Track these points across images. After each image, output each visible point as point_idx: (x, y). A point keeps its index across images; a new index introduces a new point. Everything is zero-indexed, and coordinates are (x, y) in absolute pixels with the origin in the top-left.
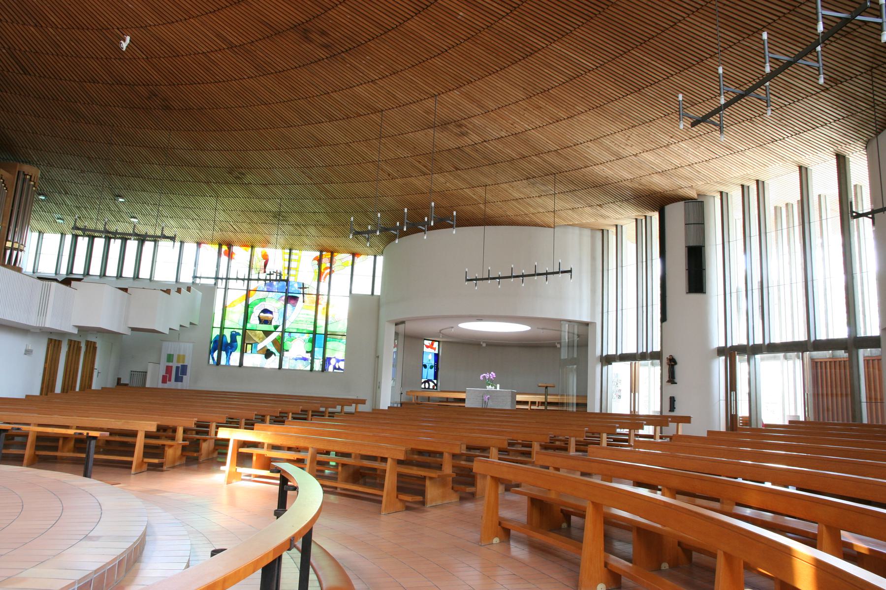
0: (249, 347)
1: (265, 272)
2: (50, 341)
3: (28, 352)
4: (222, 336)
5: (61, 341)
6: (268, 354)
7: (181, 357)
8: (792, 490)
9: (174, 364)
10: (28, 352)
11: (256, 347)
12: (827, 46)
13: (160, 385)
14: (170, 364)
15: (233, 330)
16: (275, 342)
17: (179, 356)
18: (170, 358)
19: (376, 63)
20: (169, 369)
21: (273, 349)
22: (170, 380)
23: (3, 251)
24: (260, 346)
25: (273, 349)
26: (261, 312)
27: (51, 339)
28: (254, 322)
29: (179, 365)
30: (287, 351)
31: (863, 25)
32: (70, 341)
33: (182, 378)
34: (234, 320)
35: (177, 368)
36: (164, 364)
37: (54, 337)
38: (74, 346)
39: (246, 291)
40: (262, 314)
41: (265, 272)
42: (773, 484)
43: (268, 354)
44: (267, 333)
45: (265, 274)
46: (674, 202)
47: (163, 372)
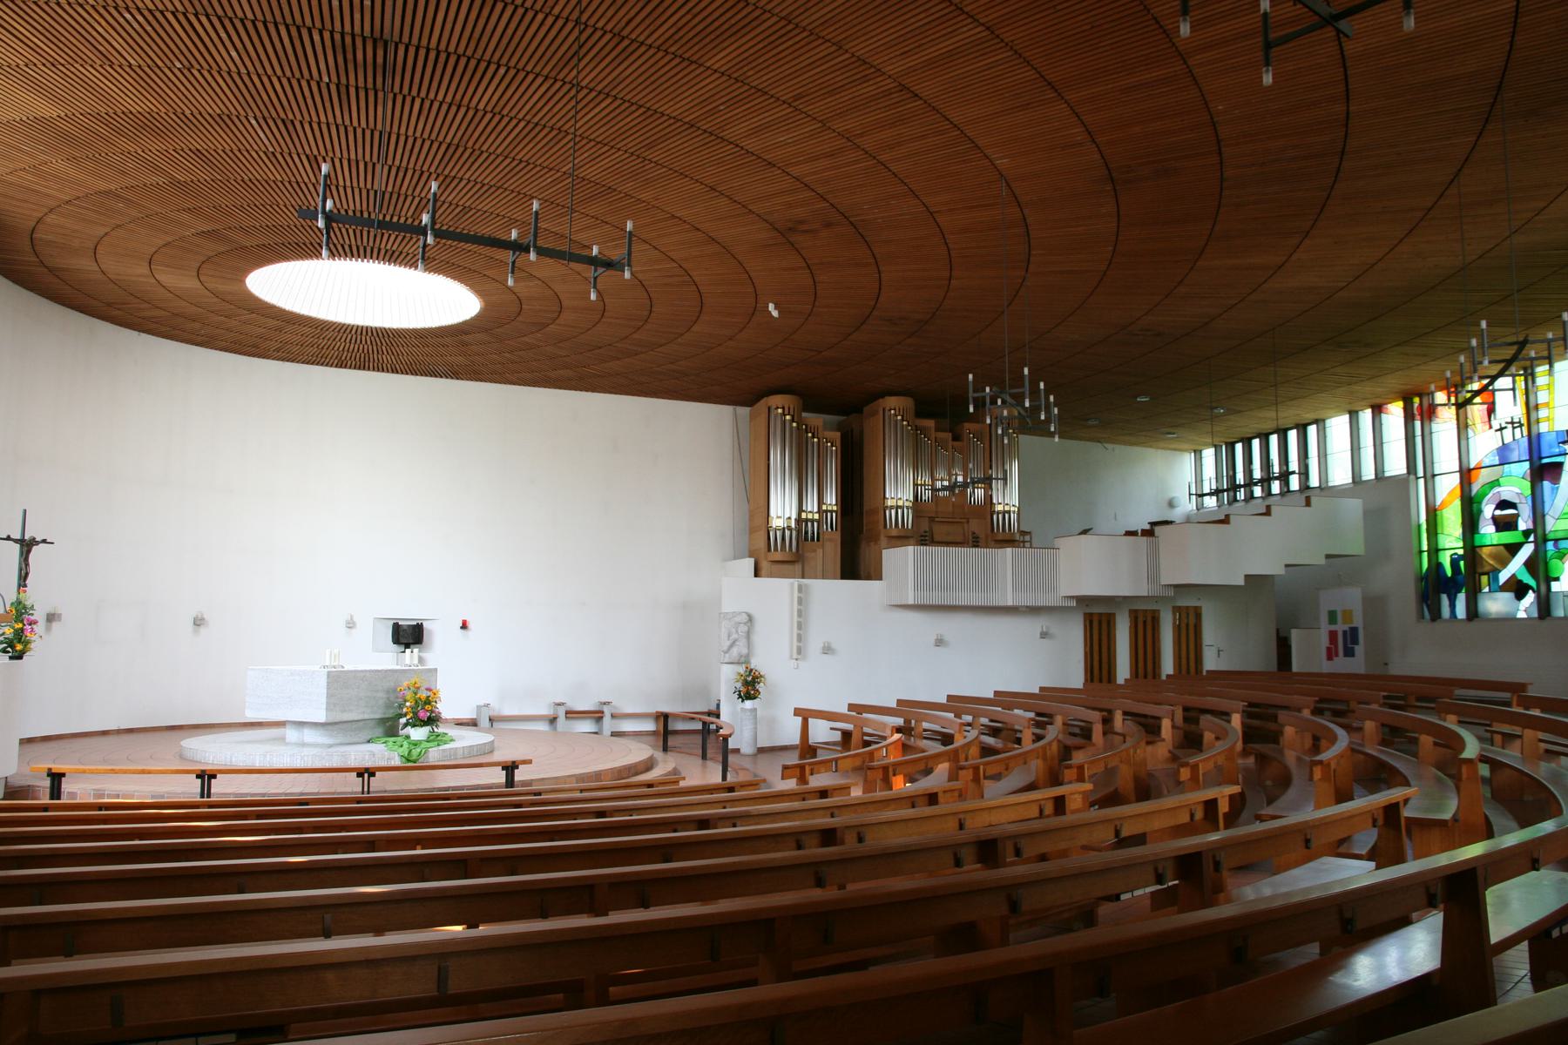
0: (1484, 579)
1: (1491, 427)
2: (1089, 620)
3: (1044, 635)
4: (1437, 567)
5: (1114, 614)
6: (1519, 589)
7: (1348, 615)
8: (1000, 709)
9: (1340, 627)
10: (1044, 635)
11: (1496, 579)
12: (228, 113)
13: (1326, 667)
14: (1333, 628)
15: (1452, 552)
16: (1530, 565)
17: (1344, 612)
18: (1332, 616)
19: (271, 215)
20: (1333, 636)
21: (1527, 579)
22: (1337, 655)
23: (989, 517)
24: (1504, 576)
25: (1527, 579)
26: (1496, 508)
27: (1136, 611)
28: (1488, 533)
29: (1346, 627)
30: (1557, 579)
31: (280, 23)
32: (1135, 616)
33: (1353, 648)
34: (1452, 539)
35: (1345, 633)
36: (1325, 628)
37: (1096, 610)
38: (1145, 624)
39: (1458, 474)
40: (1498, 512)
41: (1491, 427)
42: (1542, 712)
43: (1519, 589)
44: (1513, 549)
45: (1493, 430)
46: (426, 375)
47: (1325, 641)
